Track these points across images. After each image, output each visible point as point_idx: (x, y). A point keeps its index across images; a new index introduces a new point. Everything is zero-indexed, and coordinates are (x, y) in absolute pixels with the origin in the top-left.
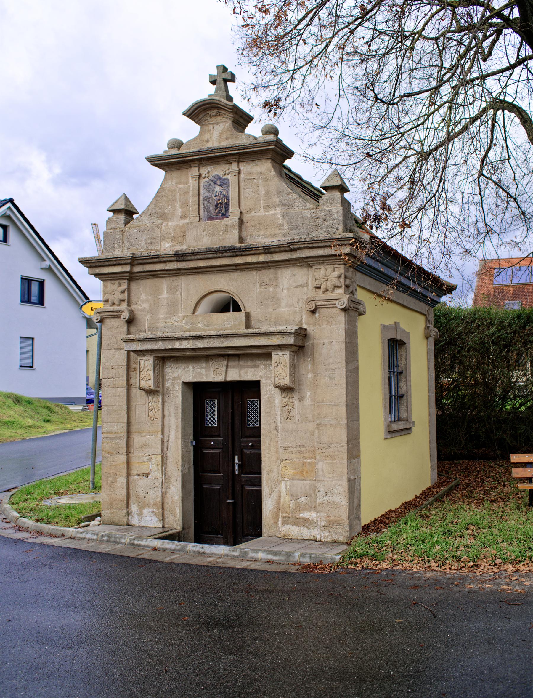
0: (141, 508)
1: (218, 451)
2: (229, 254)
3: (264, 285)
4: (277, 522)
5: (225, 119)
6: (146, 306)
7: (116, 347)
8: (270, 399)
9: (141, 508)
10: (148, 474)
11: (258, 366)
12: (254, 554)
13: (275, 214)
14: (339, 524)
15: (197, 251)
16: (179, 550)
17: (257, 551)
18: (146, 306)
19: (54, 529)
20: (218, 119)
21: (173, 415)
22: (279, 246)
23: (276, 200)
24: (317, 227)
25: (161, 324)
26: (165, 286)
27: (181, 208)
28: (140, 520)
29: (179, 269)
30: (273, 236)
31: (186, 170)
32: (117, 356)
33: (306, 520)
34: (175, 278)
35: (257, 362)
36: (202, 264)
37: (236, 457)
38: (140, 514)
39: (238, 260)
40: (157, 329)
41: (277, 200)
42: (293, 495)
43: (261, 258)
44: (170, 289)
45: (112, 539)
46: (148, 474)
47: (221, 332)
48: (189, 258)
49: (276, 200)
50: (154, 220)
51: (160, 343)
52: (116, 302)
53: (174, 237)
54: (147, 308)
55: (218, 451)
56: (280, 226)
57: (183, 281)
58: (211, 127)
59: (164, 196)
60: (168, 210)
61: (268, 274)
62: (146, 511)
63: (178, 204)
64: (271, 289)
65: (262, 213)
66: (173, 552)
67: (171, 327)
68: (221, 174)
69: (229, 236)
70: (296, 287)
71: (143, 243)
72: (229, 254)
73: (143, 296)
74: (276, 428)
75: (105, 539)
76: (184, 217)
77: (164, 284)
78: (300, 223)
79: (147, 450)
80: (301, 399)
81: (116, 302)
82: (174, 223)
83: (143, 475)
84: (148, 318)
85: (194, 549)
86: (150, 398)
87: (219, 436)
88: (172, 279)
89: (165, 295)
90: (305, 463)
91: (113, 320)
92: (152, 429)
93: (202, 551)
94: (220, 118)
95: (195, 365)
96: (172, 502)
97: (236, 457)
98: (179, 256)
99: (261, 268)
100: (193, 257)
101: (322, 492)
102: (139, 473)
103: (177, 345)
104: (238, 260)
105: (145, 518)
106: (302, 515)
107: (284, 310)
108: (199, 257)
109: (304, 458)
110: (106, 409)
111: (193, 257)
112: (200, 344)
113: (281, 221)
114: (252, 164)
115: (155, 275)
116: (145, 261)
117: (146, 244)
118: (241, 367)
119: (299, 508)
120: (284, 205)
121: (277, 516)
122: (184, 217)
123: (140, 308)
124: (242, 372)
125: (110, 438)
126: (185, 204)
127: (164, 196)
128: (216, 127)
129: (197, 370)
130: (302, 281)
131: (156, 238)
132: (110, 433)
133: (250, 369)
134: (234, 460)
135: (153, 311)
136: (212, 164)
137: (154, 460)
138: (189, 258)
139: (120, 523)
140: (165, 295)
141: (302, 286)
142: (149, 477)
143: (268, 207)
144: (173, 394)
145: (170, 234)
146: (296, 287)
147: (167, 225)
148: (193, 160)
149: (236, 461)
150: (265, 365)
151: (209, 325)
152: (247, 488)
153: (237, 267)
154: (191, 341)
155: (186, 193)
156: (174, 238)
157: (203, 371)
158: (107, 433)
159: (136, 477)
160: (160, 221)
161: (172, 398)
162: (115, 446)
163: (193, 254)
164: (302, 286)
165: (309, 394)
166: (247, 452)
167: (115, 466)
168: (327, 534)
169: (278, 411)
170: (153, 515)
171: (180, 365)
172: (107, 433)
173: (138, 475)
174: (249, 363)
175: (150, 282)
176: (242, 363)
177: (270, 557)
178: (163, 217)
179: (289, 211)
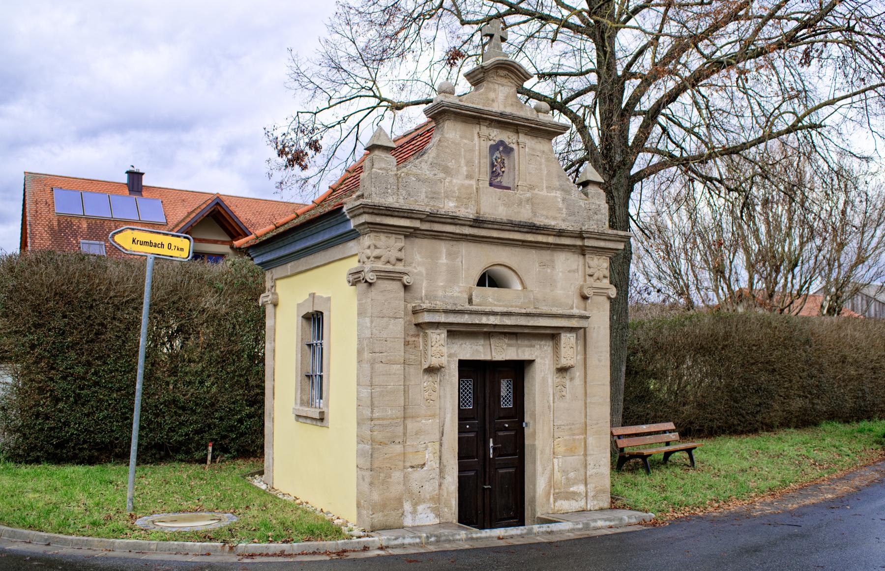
0: (415, 505)
1: (472, 435)
2: (525, 230)
3: (543, 265)
4: (548, 500)
5: (510, 84)
6: (422, 269)
7: (391, 315)
8: (544, 379)
9: (415, 505)
10: (424, 464)
11: (534, 346)
12: (530, 532)
13: (556, 197)
14: (604, 492)
15: (499, 220)
16: (527, 534)
17: (595, 521)
18: (422, 269)
19: (346, 544)
20: (504, 81)
21: (448, 396)
22: (572, 232)
23: (557, 183)
24: (589, 218)
25: (440, 293)
26: (444, 251)
27: (466, 166)
28: (414, 520)
29: (470, 235)
30: (555, 218)
31: (471, 126)
32: (391, 326)
33: (574, 493)
34: (455, 243)
35: (534, 342)
36: (495, 234)
37: (491, 440)
38: (414, 512)
39: (530, 237)
40: (435, 298)
41: (558, 183)
42: (564, 472)
43: (551, 240)
44: (449, 254)
45: (443, 538)
46: (424, 464)
47: (510, 310)
48: (486, 225)
49: (557, 183)
50: (436, 172)
51: (466, 316)
52: (393, 260)
53: (458, 197)
54: (424, 272)
55: (472, 435)
56: (560, 209)
57: (464, 248)
58: (496, 86)
59: (447, 147)
60: (451, 164)
61: (546, 255)
62: (420, 508)
63: (463, 162)
64: (549, 271)
65: (544, 193)
66: (522, 536)
67: (452, 297)
68: (507, 141)
69: (523, 210)
70: (569, 272)
71: (423, 196)
72: (525, 230)
73: (418, 258)
74: (549, 407)
75: (433, 539)
76: (469, 177)
77: (443, 248)
78: (576, 210)
79: (422, 437)
80: (572, 379)
81: (393, 260)
82: (459, 182)
83: (418, 466)
84: (424, 284)
85: (541, 530)
86: (426, 377)
87: (473, 419)
88: (451, 243)
89: (444, 260)
90: (574, 440)
91: (386, 282)
92: (429, 413)
93: (549, 530)
94: (506, 80)
95: (472, 341)
96: (448, 493)
97: (491, 440)
98: (478, 222)
99: (541, 248)
100: (490, 226)
101: (592, 465)
102: (413, 465)
103: (484, 320)
104: (530, 237)
105: (420, 516)
106: (572, 489)
107: (559, 292)
108: (496, 227)
109: (574, 434)
110: (378, 389)
111: (490, 226)
112: (508, 321)
113: (561, 205)
114: (536, 140)
115: (437, 236)
116: (437, 220)
117: (427, 197)
118: (518, 346)
119: (570, 482)
120: (563, 190)
121: (549, 494)
122: (469, 177)
123: (415, 271)
124: (520, 351)
125: (383, 426)
126: (469, 163)
127: (447, 147)
128: (501, 88)
129: (475, 347)
130: (574, 267)
131: (439, 193)
132: (383, 419)
133: (527, 349)
134: (486, 443)
135: (431, 276)
136: (500, 128)
137: (430, 449)
138: (486, 225)
139: (396, 526)
140: (444, 260)
141: (574, 271)
142: (425, 468)
143: (550, 188)
144: (449, 374)
145: (454, 192)
146: (569, 272)
147: (451, 182)
148: (486, 119)
149: (491, 444)
150: (540, 345)
151: (499, 301)
152: (501, 471)
153: (524, 244)
154: (498, 317)
155: (472, 151)
156: (459, 199)
157: (481, 348)
158: (378, 419)
159: (410, 470)
160: (442, 175)
161: (447, 377)
162: (389, 434)
163: (493, 222)
164: (574, 271)
165: (578, 374)
166: (501, 434)
167: (390, 458)
168: (595, 502)
169: (551, 391)
170: (429, 511)
171: (457, 341)
172: (378, 419)
173: (412, 467)
174: (526, 342)
175: (426, 243)
176: (519, 342)
177: (608, 523)
178: (446, 171)
179: (568, 197)
